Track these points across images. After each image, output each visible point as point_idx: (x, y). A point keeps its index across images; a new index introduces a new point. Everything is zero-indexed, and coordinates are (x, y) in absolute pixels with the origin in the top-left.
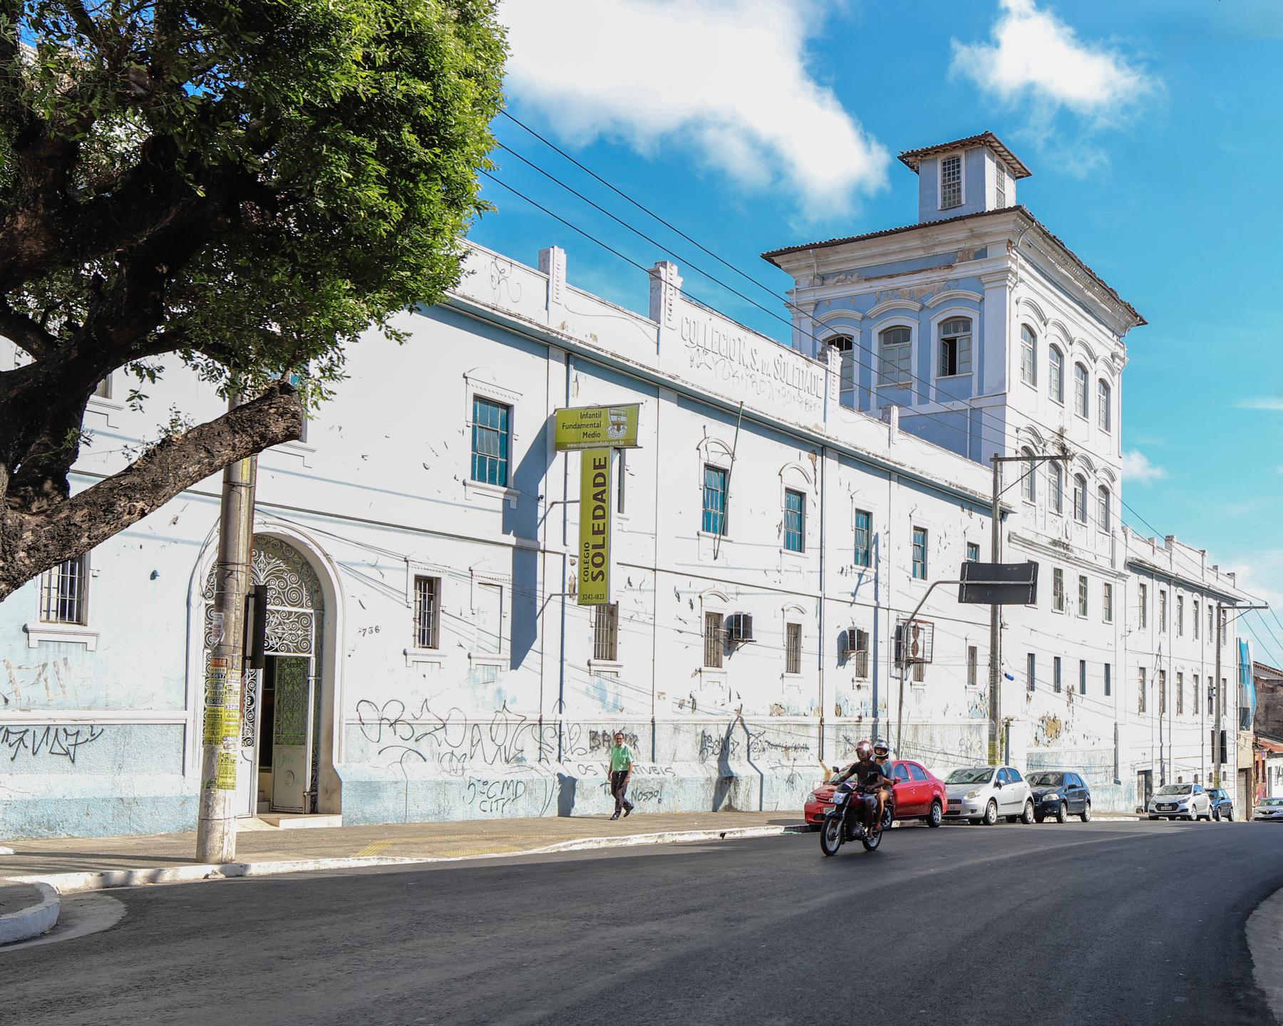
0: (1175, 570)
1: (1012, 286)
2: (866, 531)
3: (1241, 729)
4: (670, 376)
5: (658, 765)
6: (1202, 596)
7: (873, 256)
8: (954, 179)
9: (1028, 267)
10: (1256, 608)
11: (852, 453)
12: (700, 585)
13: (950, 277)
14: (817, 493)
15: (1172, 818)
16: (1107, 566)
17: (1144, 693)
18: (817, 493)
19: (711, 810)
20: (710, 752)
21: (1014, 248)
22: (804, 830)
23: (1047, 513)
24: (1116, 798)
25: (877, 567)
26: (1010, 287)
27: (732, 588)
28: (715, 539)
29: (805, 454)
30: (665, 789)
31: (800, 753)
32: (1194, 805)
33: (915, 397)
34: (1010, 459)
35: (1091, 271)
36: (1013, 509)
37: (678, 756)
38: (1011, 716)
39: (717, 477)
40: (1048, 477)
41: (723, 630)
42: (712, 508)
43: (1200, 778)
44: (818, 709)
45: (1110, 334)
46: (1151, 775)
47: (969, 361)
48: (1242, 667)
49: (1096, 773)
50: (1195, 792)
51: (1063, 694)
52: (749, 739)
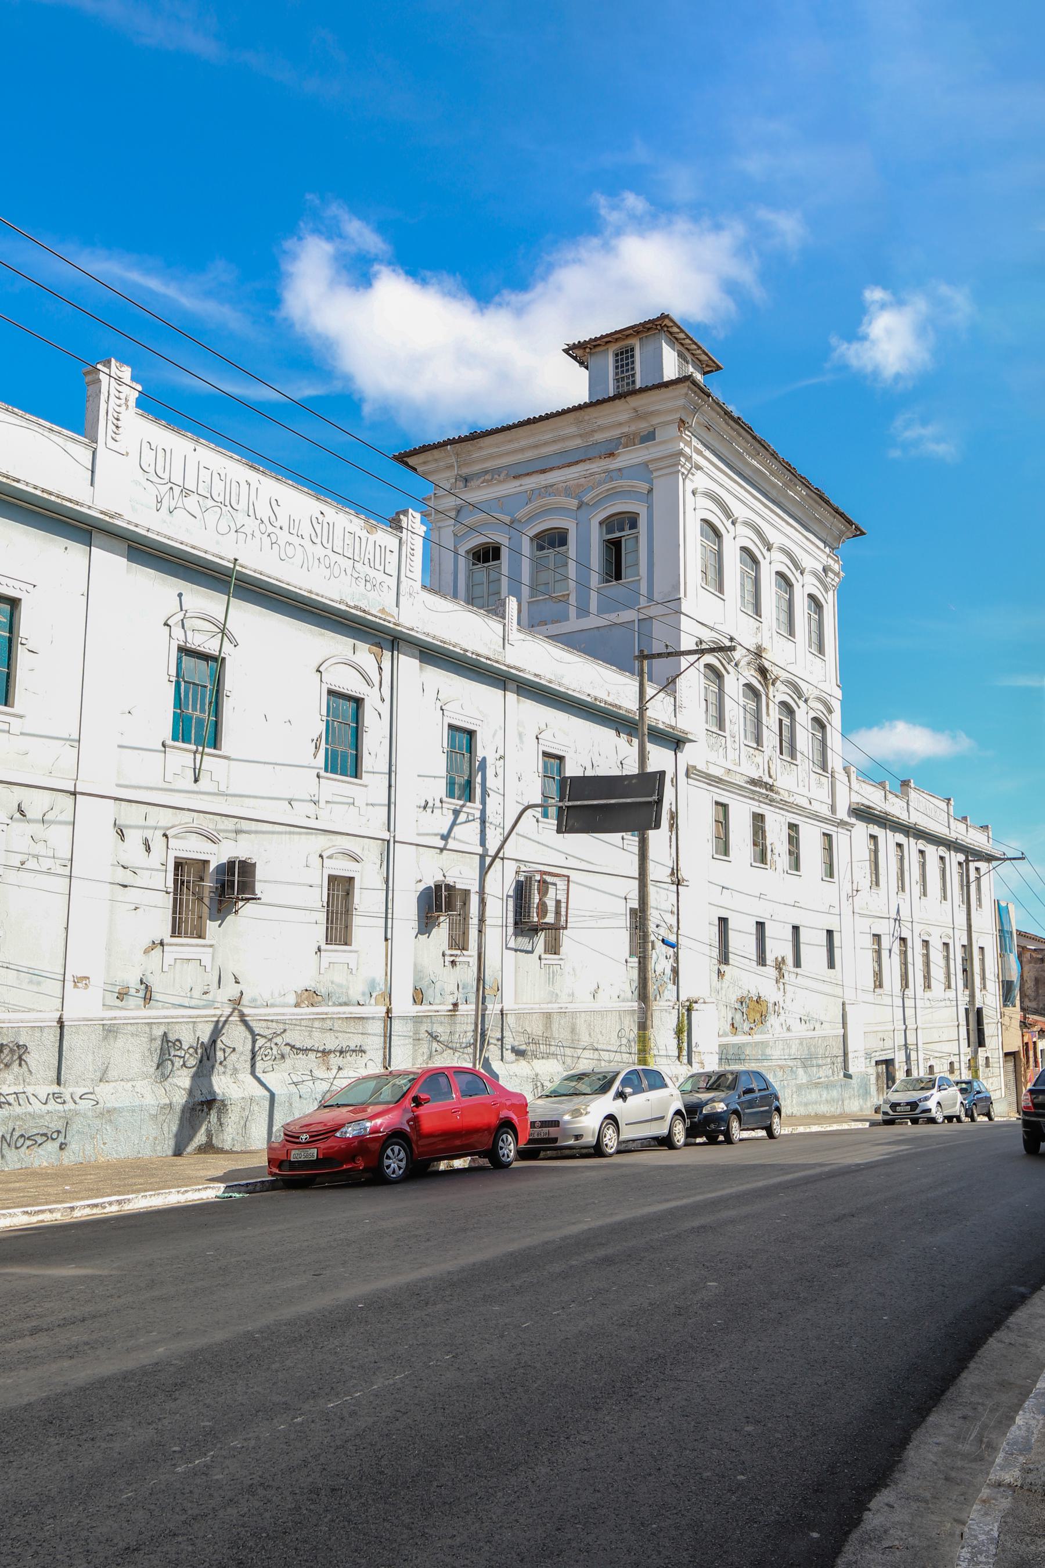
0: (916, 818)
1: (686, 473)
2: (467, 755)
3: (1005, 1005)
4: (102, 513)
5: (66, 1091)
6: (949, 851)
7: (522, 450)
8: (627, 371)
9: (707, 453)
10: (1010, 859)
11: (440, 651)
12: (165, 818)
13: (612, 467)
14: (383, 700)
15: (915, 1121)
16: (825, 811)
17: (880, 965)
18: (383, 700)
19: (170, 1152)
20: (178, 1062)
21: (686, 429)
22: (272, 1186)
23: (811, 772)
24: (846, 1095)
25: (483, 802)
26: (683, 474)
27: (229, 824)
28: (195, 753)
29: (363, 647)
30: (74, 1127)
31: (350, 1058)
32: (939, 1103)
33: (572, 611)
34: (659, 655)
35: (790, 465)
36: (690, 737)
37: (112, 1074)
38: (694, 995)
39: (199, 671)
40: (742, 703)
41: (209, 884)
42: (194, 709)
43: (956, 1066)
44: (383, 995)
45: (821, 545)
46: (893, 1065)
47: (637, 564)
48: (1003, 934)
49: (819, 1066)
50: (939, 1087)
51: (771, 971)
52: (254, 1042)
